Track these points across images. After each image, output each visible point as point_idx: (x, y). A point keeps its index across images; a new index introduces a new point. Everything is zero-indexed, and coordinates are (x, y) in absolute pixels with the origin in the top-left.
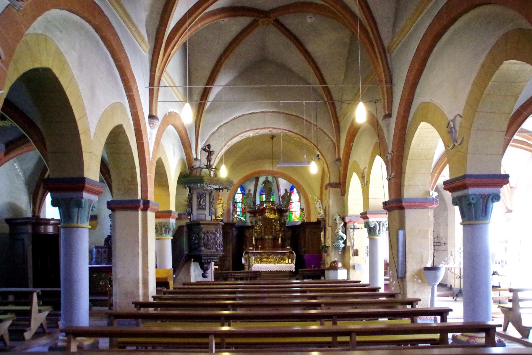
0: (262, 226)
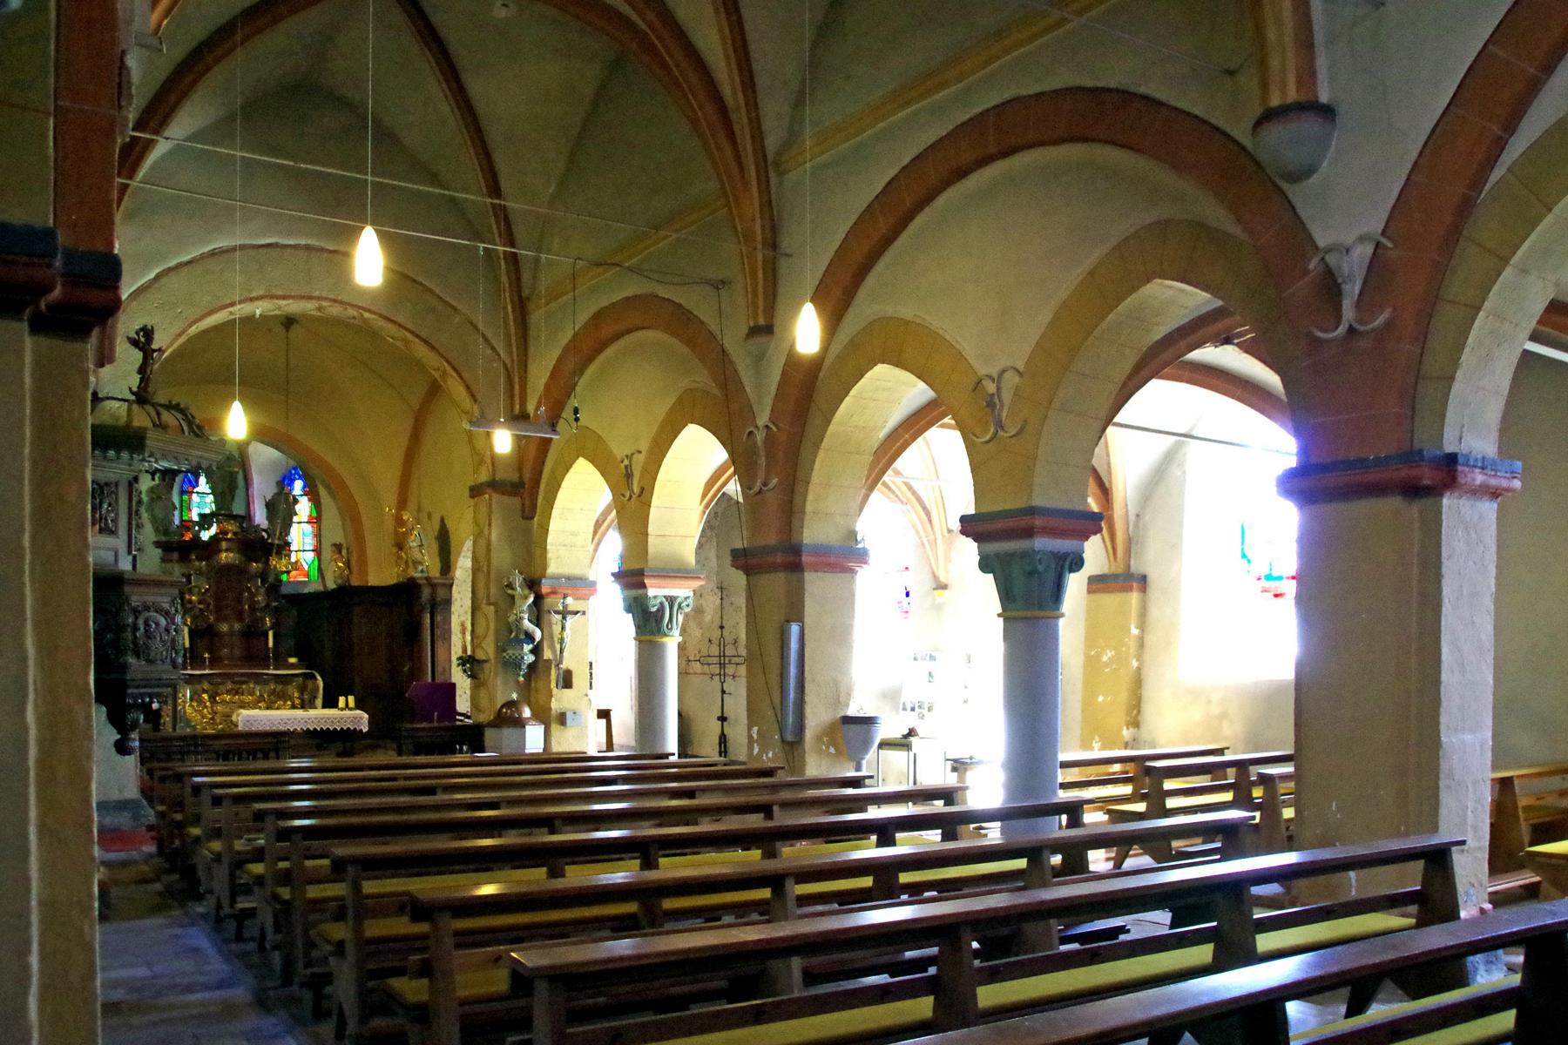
0: (207, 590)
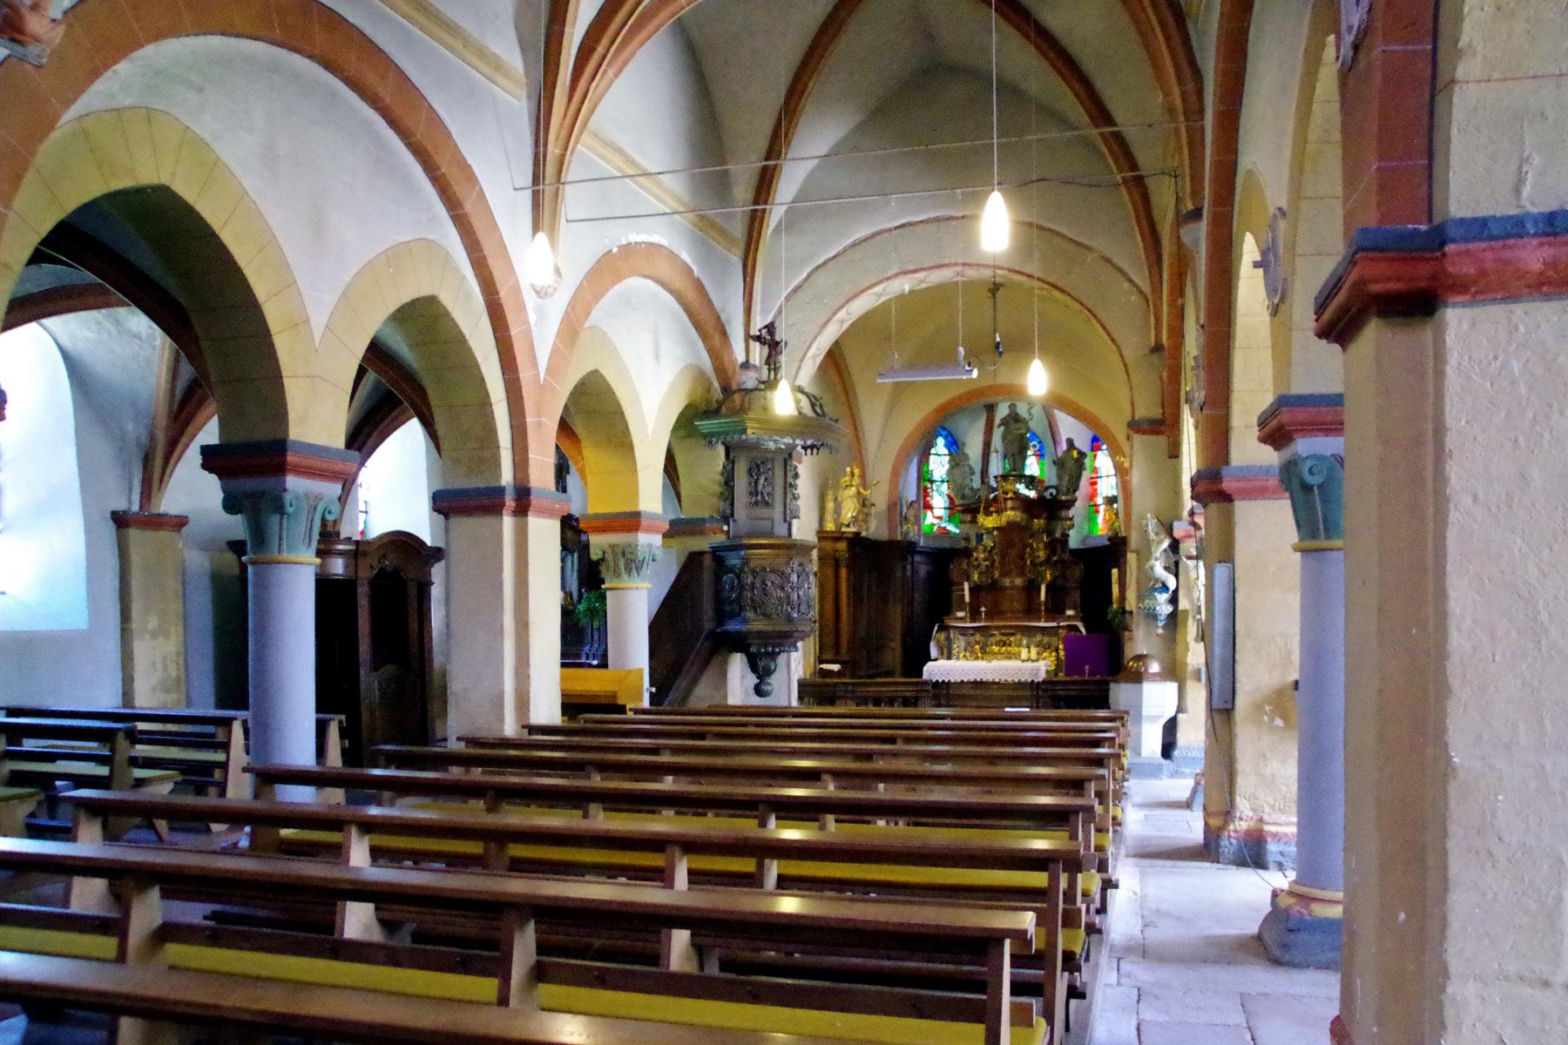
0: (992, 548)
